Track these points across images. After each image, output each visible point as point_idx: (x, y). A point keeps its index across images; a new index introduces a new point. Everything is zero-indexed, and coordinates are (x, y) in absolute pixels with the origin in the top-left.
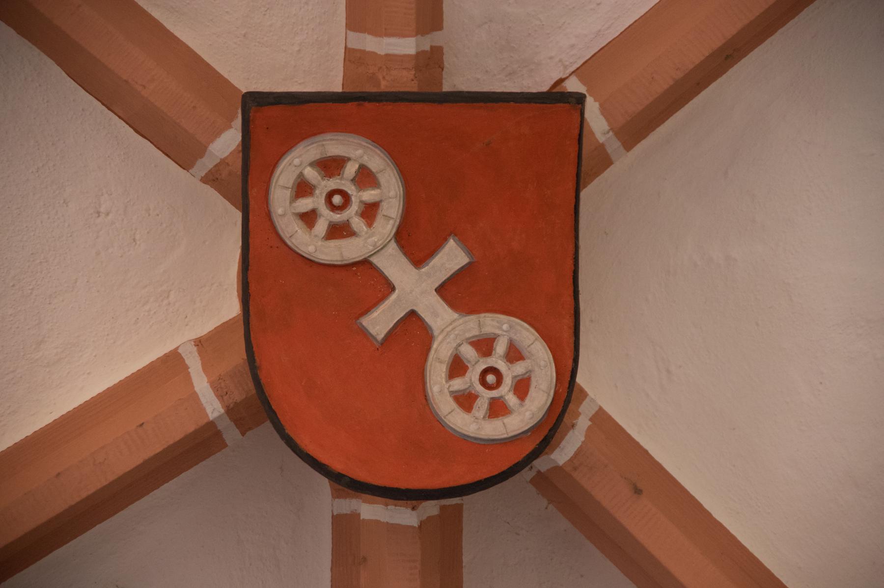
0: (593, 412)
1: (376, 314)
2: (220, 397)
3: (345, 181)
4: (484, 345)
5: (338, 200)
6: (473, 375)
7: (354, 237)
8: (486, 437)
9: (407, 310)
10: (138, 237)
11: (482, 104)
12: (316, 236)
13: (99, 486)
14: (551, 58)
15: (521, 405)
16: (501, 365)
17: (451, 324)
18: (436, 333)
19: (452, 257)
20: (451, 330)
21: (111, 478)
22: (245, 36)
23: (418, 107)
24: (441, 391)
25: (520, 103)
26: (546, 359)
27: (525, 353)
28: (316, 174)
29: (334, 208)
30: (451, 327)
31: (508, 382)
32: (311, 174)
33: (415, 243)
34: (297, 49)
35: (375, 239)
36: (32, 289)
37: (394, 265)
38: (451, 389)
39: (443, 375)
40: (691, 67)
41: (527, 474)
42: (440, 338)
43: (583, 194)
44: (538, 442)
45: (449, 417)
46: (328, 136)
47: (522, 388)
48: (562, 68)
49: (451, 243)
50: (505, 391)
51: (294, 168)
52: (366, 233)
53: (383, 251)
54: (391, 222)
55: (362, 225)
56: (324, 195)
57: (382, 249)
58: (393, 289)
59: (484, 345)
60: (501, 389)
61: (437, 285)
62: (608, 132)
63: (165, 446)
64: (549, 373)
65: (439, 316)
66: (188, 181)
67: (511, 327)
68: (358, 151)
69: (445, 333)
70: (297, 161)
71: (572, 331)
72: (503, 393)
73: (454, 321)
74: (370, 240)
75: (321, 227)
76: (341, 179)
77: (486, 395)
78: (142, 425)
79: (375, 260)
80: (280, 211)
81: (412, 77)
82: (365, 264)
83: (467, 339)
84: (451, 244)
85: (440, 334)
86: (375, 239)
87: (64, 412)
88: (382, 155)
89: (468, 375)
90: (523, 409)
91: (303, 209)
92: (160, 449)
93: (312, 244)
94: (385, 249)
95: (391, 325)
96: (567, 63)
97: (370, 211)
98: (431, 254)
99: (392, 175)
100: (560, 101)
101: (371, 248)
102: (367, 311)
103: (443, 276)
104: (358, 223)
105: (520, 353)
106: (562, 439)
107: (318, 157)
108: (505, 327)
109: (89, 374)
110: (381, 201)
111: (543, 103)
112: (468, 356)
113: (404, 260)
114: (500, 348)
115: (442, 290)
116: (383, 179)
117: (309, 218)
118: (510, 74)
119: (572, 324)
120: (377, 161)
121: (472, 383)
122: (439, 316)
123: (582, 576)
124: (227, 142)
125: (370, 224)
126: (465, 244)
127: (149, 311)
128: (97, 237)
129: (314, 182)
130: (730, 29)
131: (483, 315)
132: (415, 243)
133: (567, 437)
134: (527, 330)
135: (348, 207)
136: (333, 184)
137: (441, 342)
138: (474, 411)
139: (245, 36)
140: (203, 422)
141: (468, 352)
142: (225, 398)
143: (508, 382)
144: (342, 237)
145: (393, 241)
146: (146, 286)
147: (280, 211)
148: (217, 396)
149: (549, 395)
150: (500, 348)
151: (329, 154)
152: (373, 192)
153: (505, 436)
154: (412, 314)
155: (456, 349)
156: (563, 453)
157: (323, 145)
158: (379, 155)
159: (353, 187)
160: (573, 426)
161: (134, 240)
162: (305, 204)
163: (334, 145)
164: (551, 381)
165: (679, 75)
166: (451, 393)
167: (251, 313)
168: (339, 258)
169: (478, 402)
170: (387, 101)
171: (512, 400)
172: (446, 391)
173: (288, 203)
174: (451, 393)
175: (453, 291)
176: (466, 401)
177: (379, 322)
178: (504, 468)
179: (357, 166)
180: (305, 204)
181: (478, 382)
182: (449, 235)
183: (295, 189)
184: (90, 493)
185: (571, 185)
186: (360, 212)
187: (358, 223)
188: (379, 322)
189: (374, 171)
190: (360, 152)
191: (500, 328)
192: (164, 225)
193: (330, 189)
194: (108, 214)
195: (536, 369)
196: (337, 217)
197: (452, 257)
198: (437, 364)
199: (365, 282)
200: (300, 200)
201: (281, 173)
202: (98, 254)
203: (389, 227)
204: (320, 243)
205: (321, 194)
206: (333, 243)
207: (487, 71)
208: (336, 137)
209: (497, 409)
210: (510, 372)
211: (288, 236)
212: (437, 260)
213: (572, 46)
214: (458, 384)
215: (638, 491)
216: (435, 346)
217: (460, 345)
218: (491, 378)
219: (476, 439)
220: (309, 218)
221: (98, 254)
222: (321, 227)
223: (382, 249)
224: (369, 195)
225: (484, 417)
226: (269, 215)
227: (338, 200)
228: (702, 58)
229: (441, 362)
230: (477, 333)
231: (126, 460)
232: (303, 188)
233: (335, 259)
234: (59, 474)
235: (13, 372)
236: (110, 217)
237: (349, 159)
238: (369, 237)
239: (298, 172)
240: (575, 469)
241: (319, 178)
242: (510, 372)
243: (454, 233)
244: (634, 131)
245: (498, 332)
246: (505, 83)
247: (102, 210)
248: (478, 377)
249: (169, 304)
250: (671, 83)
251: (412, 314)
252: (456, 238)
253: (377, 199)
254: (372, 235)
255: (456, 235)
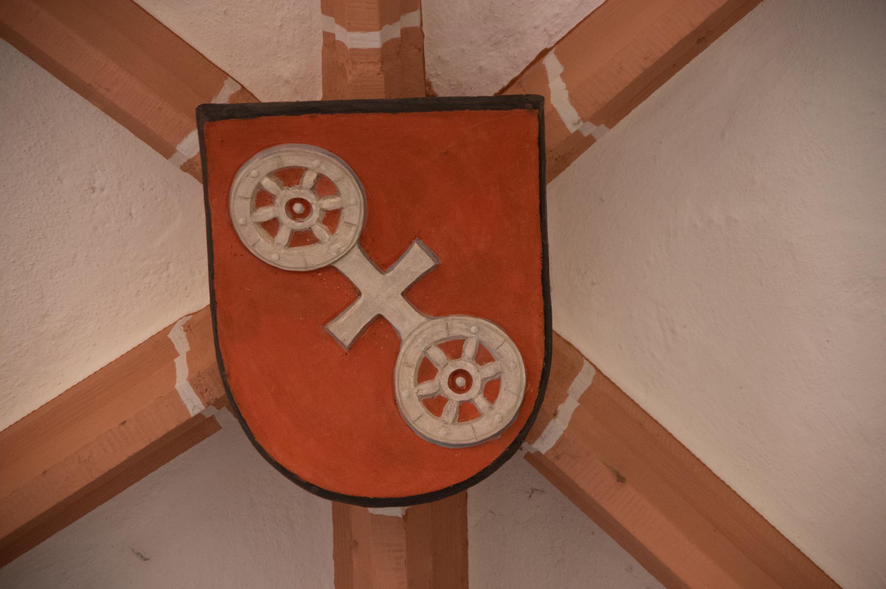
0: (585, 388)
1: (343, 319)
2: (201, 394)
3: (304, 189)
4: (453, 348)
5: (299, 209)
6: (442, 378)
7: (317, 244)
8: (454, 443)
9: (374, 315)
10: (133, 211)
11: (437, 112)
12: (279, 244)
13: (85, 483)
14: (536, 27)
15: (491, 408)
16: (470, 368)
17: (418, 328)
18: (403, 337)
19: (416, 261)
20: (418, 333)
21: (97, 475)
22: (225, 13)
23: (371, 117)
24: (410, 396)
25: (475, 109)
26: (516, 361)
27: (494, 354)
28: (275, 184)
29: (295, 216)
30: (418, 331)
31: (477, 384)
32: (269, 184)
33: (380, 248)
34: (279, 24)
35: (338, 245)
36: (33, 265)
37: (358, 270)
38: (420, 393)
39: (412, 380)
40: (660, 55)
41: (519, 455)
42: (408, 342)
43: (552, 189)
44: (508, 445)
45: (417, 422)
46: (283, 148)
47: (492, 390)
48: (547, 37)
49: (416, 247)
50: (475, 394)
51: (252, 180)
52: (329, 240)
53: (347, 257)
54: (354, 229)
55: (324, 232)
56: (284, 204)
57: (346, 254)
58: (360, 294)
59: (453, 348)
60: (470, 391)
61: (403, 289)
62: (578, 123)
63: (148, 444)
64: (519, 374)
65: (407, 320)
66: (170, 169)
67: (479, 329)
68: (315, 161)
69: (412, 337)
70: (254, 173)
71: (542, 330)
72: (472, 396)
73: (422, 324)
74: (333, 247)
75: (283, 235)
76: (300, 188)
77: (455, 398)
78: (124, 423)
79: (339, 266)
80: (241, 221)
81: (378, 71)
82: (330, 270)
83: (435, 342)
84: (416, 248)
85: (408, 338)
86: (338, 245)
87: (68, 386)
88: (340, 164)
89: (437, 377)
90: (492, 412)
91: (265, 219)
92: (143, 447)
93: (275, 251)
94: (349, 255)
95: (358, 331)
96: (552, 33)
97: (332, 218)
98: (397, 256)
99: (351, 183)
100: (520, 103)
101: (335, 254)
102: (334, 316)
103: (409, 281)
104: (320, 231)
105: (489, 354)
106: (544, 427)
107: (275, 168)
108: (473, 329)
109: (94, 345)
110: (342, 208)
111: (498, 109)
112: (437, 360)
113: (369, 266)
114: (469, 350)
115: (408, 294)
116: (341, 187)
117: (271, 226)
118: (496, 43)
119: (542, 324)
120: (334, 170)
121: (440, 387)
122: (407, 320)
123: (593, 533)
124: (190, 145)
125: (332, 231)
126: (431, 248)
127: (150, 283)
128: (94, 213)
129: (273, 192)
130: (698, 18)
131: (450, 318)
132: (380, 248)
133: (549, 427)
134: (496, 332)
135: (312, 214)
136: (292, 193)
137: (409, 346)
138: (443, 415)
139: (225, 13)
140: (184, 419)
141: (437, 356)
142: (205, 395)
143: (477, 384)
144: (305, 243)
145: (356, 247)
146: (145, 259)
147: (241, 221)
148: (197, 393)
149: (518, 397)
150: (469, 350)
151: (286, 165)
152: (333, 200)
153: (474, 441)
154: (379, 319)
155: (425, 352)
156: (544, 444)
157: (279, 157)
158: (336, 165)
159: (313, 196)
160: (555, 415)
161: (130, 214)
162: (266, 213)
163: (290, 156)
164: (521, 383)
165: (648, 64)
166: (420, 397)
167: (218, 321)
168: (303, 265)
169: (448, 406)
170: (339, 112)
171: (481, 403)
172: (415, 395)
173: (248, 212)
174: (420, 397)
175: (419, 295)
176: (435, 405)
177: (346, 327)
178: (473, 473)
179: (315, 175)
180: (266, 213)
181: (447, 386)
182: (414, 239)
183: (255, 198)
184: (77, 489)
185: (534, 187)
186: (321, 219)
187: (320, 231)
188: (346, 327)
189: (333, 179)
190: (316, 162)
191: (468, 330)
192: (159, 199)
193: (289, 198)
194: (102, 190)
195: (506, 371)
196: (299, 225)
197: (416, 261)
198: (406, 368)
199: (330, 289)
200: (260, 209)
201: (239, 183)
202: (95, 229)
203: (352, 233)
204: (283, 251)
205: (281, 203)
206: (296, 250)
207: (471, 42)
208: (292, 149)
209: (467, 412)
210: (480, 374)
211: (251, 244)
212: (401, 265)
213: (557, 16)
214: (427, 388)
215: (621, 479)
216: (403, 350)
217: (428, 348)
218: (460, 381)
219: (444, 444)
220: (271, 226)
221: (95, 229)
222: (283, 235)
223: (346, 254)
224: (330, 203)
225: (453, 422)
226: (231, 224)
227: (299, 209)
228: (671, 47)
229: (409, 366)
230: (445, 336)
231: (110, 459)
232: (262, 198)
233: (299, 266)
234: (45, 472)
235: (19, 345)
236: (105, 192)
237: (306, 169)
238: (332, 244)
239: (256, 183)
240: (558, 457)
241: (278, 188)
242: (480, 374)
243: (418, 236)
244: (613, 112)
245: (465, 334)
246: (491, 53)
247: (97, 185)
248: (447, 380)
249: (169, 276)
250: (640, 72)
251: (380, 318)
252: (421, 241)
253: (338, 207)
254: (335, 242)
255: (420, 238)
